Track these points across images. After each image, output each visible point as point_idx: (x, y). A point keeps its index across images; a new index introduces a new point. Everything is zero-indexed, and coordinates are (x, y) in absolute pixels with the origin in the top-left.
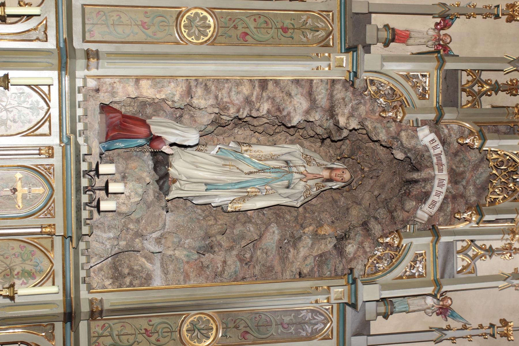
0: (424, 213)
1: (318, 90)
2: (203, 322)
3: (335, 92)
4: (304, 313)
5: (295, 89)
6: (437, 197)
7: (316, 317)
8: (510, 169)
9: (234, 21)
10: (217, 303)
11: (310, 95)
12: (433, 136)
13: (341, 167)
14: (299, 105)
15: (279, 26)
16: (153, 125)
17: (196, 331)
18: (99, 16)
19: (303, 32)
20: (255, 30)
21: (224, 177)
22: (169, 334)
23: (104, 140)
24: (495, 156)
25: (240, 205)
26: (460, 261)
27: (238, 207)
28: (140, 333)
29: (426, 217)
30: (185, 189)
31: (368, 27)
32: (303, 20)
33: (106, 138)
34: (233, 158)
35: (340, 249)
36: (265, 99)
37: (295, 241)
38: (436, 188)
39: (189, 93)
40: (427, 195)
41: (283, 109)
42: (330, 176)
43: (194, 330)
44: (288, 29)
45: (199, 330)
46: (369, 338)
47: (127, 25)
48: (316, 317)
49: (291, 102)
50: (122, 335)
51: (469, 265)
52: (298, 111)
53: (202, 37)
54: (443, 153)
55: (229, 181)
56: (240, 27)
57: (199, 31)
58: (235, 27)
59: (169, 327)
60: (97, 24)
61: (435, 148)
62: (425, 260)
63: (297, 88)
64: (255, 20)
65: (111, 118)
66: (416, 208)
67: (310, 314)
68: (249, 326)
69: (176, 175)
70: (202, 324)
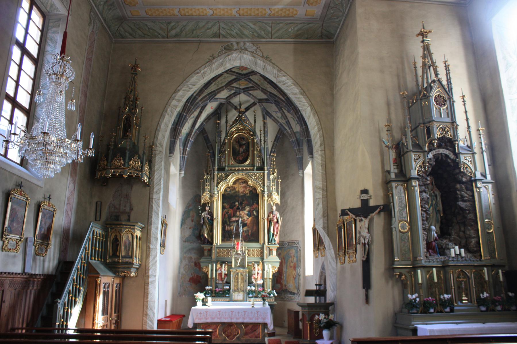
0: (452, 156)
6: (447, 152)
12: (430, 153)
29: (453, 156)
35: (463, 183)
37: (463, 197)
38: (445, 153)
40: (446, 155)
66: (450, 158)
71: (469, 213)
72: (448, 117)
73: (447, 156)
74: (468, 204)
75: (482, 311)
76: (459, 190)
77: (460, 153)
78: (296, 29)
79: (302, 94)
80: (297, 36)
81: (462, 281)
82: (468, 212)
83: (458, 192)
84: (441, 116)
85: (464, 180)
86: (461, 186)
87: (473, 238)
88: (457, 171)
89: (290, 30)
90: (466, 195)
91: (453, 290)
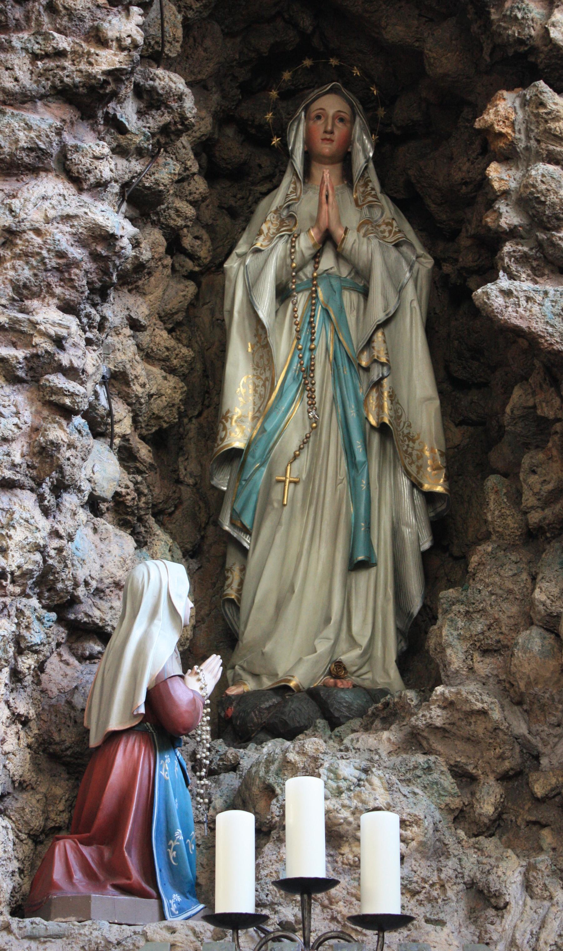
13: (302, 128)
14: (47, 204)
16: (107, 721)
21: (328, 499)
25: (427, 453)
27: (434, 459)
30: (369, 634)
33: (144, 895)
34: (264, 470)
41: (61, 255)
42: (330, 160)
49: (38, 232)
52: (71, 211)
55: (344, 486)
65: (69, 874)
69: (317, 662)
76: (509, 157)
83: (499, 175)
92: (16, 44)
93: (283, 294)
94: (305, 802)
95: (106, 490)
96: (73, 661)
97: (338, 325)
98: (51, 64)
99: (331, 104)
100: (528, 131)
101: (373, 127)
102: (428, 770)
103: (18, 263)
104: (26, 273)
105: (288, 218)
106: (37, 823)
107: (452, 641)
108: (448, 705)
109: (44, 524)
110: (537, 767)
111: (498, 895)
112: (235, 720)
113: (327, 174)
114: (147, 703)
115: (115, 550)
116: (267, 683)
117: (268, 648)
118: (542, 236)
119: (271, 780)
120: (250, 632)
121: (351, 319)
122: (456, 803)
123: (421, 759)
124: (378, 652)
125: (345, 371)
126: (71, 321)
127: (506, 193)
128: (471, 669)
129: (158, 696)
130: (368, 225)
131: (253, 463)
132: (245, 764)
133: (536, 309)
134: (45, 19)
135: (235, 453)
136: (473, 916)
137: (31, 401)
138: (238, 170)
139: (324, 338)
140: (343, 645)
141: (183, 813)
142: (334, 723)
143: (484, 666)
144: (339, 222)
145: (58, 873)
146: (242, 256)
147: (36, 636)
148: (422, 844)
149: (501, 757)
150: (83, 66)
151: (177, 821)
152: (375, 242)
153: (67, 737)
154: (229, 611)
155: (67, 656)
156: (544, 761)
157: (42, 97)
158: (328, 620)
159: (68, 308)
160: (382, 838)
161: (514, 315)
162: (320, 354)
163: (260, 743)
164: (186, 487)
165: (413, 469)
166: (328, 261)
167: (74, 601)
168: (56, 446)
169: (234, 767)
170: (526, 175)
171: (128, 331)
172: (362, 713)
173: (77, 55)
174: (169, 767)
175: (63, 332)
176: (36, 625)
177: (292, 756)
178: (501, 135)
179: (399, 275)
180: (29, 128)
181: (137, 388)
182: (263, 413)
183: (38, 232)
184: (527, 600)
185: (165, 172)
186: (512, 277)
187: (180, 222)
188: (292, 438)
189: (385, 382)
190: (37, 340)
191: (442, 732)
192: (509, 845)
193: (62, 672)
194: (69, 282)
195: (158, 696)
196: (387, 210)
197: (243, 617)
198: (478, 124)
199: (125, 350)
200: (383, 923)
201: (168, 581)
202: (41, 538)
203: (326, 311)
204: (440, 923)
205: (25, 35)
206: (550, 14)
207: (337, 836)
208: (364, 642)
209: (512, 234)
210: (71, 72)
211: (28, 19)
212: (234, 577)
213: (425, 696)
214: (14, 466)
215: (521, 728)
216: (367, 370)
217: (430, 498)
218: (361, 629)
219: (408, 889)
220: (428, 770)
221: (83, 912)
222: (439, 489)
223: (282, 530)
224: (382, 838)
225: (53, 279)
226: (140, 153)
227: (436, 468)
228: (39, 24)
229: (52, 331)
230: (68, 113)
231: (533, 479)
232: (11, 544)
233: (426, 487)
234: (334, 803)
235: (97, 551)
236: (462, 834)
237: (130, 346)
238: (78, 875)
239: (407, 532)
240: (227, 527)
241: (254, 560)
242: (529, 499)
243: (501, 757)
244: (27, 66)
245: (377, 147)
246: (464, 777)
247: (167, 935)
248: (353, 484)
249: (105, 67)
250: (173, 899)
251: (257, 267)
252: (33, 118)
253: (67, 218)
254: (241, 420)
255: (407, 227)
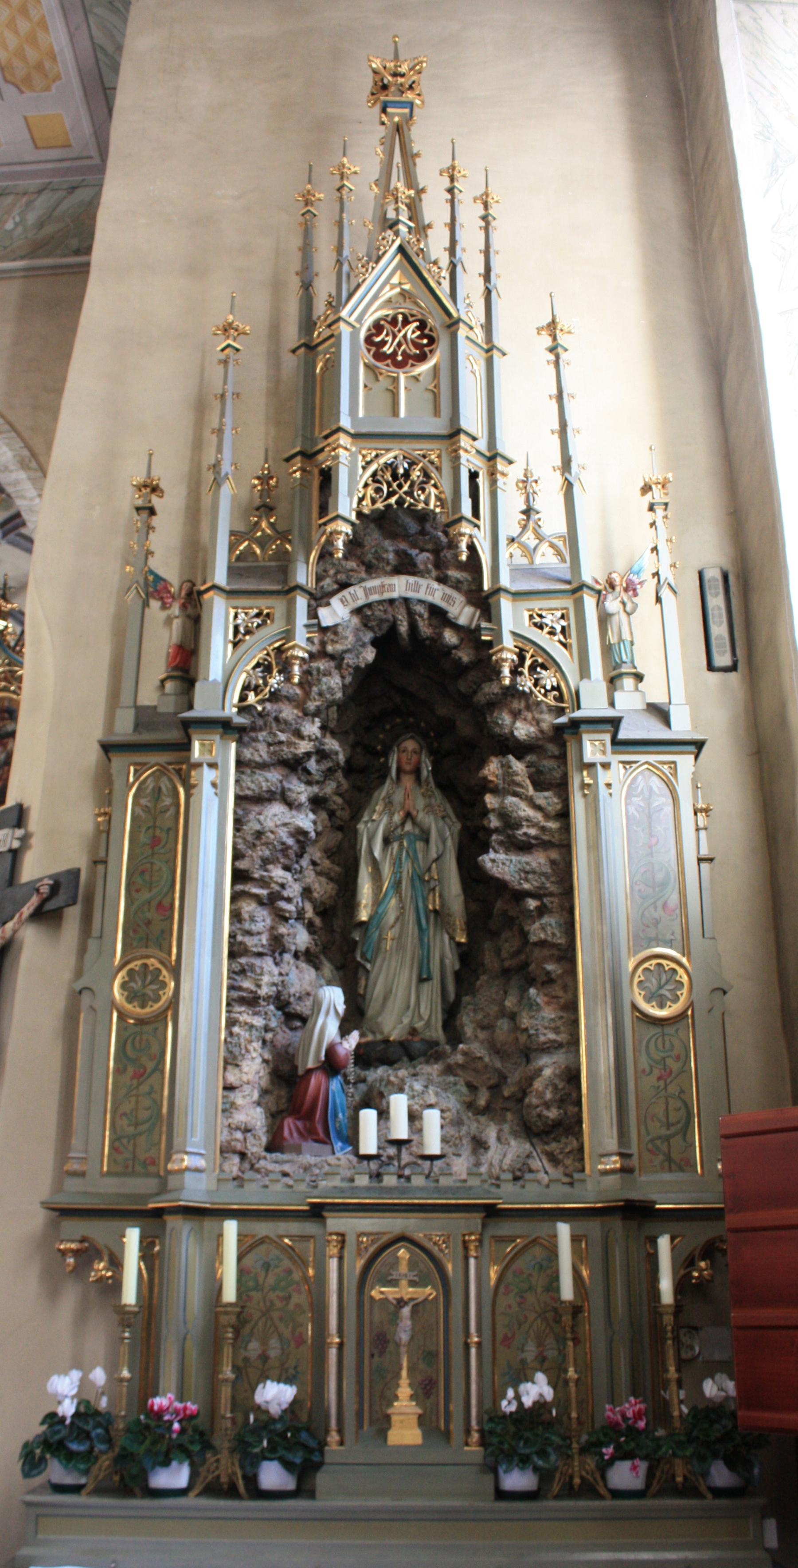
0: (463, 613)
1: (253, 786)
2: (647, 980)
3: (258, 759)
4: (632, 810)
5: (251, 824)
7: (640, 789)
8: (388, 476)
9: (139, 925)
10: (452, 1407)
11: (261, 799)
12: (335, 601)
14: (276, 819)
15: (150, 852)
17: (663, 991)
18: (122, 1148)
19: (161, 812)
20: (155, 891)
22: (667, 1038)
23: (328, 1147)
24: (367, 502)
26: (546, 558)
28: (665, 1088)
29: (469, 610)
31: (161, 710)
32: (141, 813)
35: (521, 749)
36: (265, 874)
37: (510, 822)
38: (422, 595)
39: (252, 1001)
41: (283, 843)
42: (410, 773)
43: (661, 996)
44: (154, 837)
45: (660, 987)
46: (673, 702)
47: (137, 1102)
48: (640, 789)
49: (272, 832)
50: (667, 1118)
51: (552, 545)
52: (287, 821)
53: (161, 978)
54: (363, 584)
55: (416, 941)
56: (149, 915)
57: (151, 983)
58: (148, 923)
59: (653, 1040)
60: (134, 1152)
61: (355, 598)
62: (540, 609)
63: (249, 821)
64: (138, 891)
65: (291, 1133)
67: (634, 799)
68: (655, 903)
70: (651, 982)
71: (542, 911)
72: (437, 412)
73: (438, 614)
74: (538, 860)
75: (501, 1495)
76: (495, 791)
77: (497, 591)
78: (32, 218)
79: (23, 465)
80: (36, 249)
81: (401, 1303)
82: (532, 904)
83: (490, 800)
84: (395, 412)
85: (523, 730)
86: (507, 766)
87: (549, 1048)
88: (491, 689)
89: (10, 225)
90: (530, 812)
91: (333, 1353)
92: (261, 738)
93: (387, 842)
94: (399, 1104)
95: (302, 947)
96: (287, 1030)
97: (414, 860)
98: (277, 748)
99: (410, 745)
100: (504, 780)
101: (432, 752)
102: (455, 1084)
103: (264, 848)
104: (267, 853)
105: (389, 803)
106: (274, 1109)
107: (467, 1022)
108: (465, 1054)
109: (276, 970)
110: (505, 1083)
111: (486, 1143)
112: (365, 1057)
113: (408, 781)
114: (326, 1055)
115: (307, 977)
116: (379, 1037)
117: (380, 1019)
118: (510, 832)
119: (382, 1089)
120: (371, 1011)
121: (420, 856)
122: (468, 1099)
123: (452, 1079)
124: (433, 1021)
125: (417, 883)
126: (288, 875)
127: (493, 810)
128: (476, 1037)
129: (331, 1051)
130: (429, 807)
131: (372, 929)
132: (370, 1079)
133: (506, 869)
134: (274, 725)
135: (363, 923)
136: (474, 1152)
137: (270, 914)
138: (362, 776)
139: (407, 868)
140: (416, 1019)
141: (342, 1104)
142: (412, 1058)
143: (482, 1035)
144: (414, 808)
145: (286, 1133)
146: (366, 823)
147: (273, 1024)
148: (451, 1120)
149: (489, 1079)
150: (292, 750)
151: (339, 1110)
152: (432, 817)
153: (285, 1068)
154: (359, 1000)
155: (285, 1028)
156: (509, 1080)
157: (273, 765)
158: (408, 1007)
159: (287, 868)
160: (432, 1119)
161: (496, 871)
162: (405, 875)
163: (376, 1067)
164: (341, 945)
165: (450, 931)
166: (408, 827)
167: (288, 1003)
168: (282, 936)
169: (364, 1081)
170: (502, 802)
171: (311, 867)
172: (424, 1054)
173: (290, 744)
174: (335, 1084)
175: (285, 881)
176: (273, 1019)
177: (392, 1078)
178: (491, 781)
179: (443, 833)
180: (267, 780)
181: (315, 895)
182: (378, 901)
183: (272, 832)
184: (501, 1004)
185: (329, 788)
186: (496, 852)
187: (335, 807)
188: (391, 917)
189: (437, 889)
190: (273, 885)
191: (462, 1067)
192: (492, 1119)
193: (284, 1036)
194: (286, 856)
195: (331, 1051)
196: (438, 798)
197: (367, 1001)
198: (480, 775)
199: (310, 876)
200: (432, 1158)
201: (334, 997)
202: (277, 979)
203: (407, 852)
204: (459, 1155)
205: (264, 733)
206: (514, 723)
207: (414, 1117)
208: (426, 1017)
209: (496, 830)
210: (286, 752)
211: (265, 725)
212: (363, 982)
213: (454, 1047)
214: (263, 946)
215: (498, 1064)
216: (428, 882)
217: (459, 944)
218: (424, 1010)
219: (444, 1140)
220: (455, 1084)
221: (298, 1151)
222: (463, 940)
223: (386, 963)
224: (432, 1119)
225: (280, 855)
226: (318, 782)
227: (462, 930)
228: (271, 728)
229: (280, 881)
230: (285, 771)
231: (507, 945)
232: (263, 983)
233: (457, 939)
234: (412, 1102)
235: (300, 978)
236: (470, 1114)
237: (312, 874)
238: (295, 1134)
239: (447, 962)
240: (359, 959)
241: (372, 976)
242: (504, 954)
243: (489, 1079)
244: (266, 749)
245: (434, 764)
246: (472, 1088)
247: (336, 1162)
248: (421, 939)
249: (303, 750)
250: (338, 1145)
251: (374, 827)
252: (269, 775)
253: (285, 825)
254: (366, 906)
255: (448, 807)
